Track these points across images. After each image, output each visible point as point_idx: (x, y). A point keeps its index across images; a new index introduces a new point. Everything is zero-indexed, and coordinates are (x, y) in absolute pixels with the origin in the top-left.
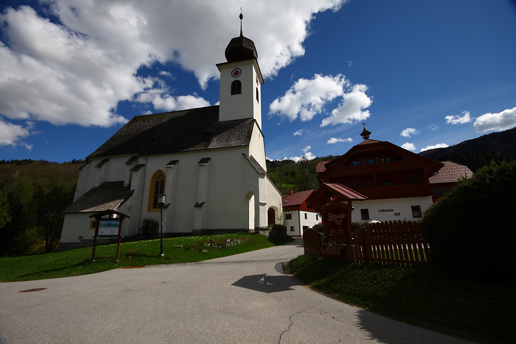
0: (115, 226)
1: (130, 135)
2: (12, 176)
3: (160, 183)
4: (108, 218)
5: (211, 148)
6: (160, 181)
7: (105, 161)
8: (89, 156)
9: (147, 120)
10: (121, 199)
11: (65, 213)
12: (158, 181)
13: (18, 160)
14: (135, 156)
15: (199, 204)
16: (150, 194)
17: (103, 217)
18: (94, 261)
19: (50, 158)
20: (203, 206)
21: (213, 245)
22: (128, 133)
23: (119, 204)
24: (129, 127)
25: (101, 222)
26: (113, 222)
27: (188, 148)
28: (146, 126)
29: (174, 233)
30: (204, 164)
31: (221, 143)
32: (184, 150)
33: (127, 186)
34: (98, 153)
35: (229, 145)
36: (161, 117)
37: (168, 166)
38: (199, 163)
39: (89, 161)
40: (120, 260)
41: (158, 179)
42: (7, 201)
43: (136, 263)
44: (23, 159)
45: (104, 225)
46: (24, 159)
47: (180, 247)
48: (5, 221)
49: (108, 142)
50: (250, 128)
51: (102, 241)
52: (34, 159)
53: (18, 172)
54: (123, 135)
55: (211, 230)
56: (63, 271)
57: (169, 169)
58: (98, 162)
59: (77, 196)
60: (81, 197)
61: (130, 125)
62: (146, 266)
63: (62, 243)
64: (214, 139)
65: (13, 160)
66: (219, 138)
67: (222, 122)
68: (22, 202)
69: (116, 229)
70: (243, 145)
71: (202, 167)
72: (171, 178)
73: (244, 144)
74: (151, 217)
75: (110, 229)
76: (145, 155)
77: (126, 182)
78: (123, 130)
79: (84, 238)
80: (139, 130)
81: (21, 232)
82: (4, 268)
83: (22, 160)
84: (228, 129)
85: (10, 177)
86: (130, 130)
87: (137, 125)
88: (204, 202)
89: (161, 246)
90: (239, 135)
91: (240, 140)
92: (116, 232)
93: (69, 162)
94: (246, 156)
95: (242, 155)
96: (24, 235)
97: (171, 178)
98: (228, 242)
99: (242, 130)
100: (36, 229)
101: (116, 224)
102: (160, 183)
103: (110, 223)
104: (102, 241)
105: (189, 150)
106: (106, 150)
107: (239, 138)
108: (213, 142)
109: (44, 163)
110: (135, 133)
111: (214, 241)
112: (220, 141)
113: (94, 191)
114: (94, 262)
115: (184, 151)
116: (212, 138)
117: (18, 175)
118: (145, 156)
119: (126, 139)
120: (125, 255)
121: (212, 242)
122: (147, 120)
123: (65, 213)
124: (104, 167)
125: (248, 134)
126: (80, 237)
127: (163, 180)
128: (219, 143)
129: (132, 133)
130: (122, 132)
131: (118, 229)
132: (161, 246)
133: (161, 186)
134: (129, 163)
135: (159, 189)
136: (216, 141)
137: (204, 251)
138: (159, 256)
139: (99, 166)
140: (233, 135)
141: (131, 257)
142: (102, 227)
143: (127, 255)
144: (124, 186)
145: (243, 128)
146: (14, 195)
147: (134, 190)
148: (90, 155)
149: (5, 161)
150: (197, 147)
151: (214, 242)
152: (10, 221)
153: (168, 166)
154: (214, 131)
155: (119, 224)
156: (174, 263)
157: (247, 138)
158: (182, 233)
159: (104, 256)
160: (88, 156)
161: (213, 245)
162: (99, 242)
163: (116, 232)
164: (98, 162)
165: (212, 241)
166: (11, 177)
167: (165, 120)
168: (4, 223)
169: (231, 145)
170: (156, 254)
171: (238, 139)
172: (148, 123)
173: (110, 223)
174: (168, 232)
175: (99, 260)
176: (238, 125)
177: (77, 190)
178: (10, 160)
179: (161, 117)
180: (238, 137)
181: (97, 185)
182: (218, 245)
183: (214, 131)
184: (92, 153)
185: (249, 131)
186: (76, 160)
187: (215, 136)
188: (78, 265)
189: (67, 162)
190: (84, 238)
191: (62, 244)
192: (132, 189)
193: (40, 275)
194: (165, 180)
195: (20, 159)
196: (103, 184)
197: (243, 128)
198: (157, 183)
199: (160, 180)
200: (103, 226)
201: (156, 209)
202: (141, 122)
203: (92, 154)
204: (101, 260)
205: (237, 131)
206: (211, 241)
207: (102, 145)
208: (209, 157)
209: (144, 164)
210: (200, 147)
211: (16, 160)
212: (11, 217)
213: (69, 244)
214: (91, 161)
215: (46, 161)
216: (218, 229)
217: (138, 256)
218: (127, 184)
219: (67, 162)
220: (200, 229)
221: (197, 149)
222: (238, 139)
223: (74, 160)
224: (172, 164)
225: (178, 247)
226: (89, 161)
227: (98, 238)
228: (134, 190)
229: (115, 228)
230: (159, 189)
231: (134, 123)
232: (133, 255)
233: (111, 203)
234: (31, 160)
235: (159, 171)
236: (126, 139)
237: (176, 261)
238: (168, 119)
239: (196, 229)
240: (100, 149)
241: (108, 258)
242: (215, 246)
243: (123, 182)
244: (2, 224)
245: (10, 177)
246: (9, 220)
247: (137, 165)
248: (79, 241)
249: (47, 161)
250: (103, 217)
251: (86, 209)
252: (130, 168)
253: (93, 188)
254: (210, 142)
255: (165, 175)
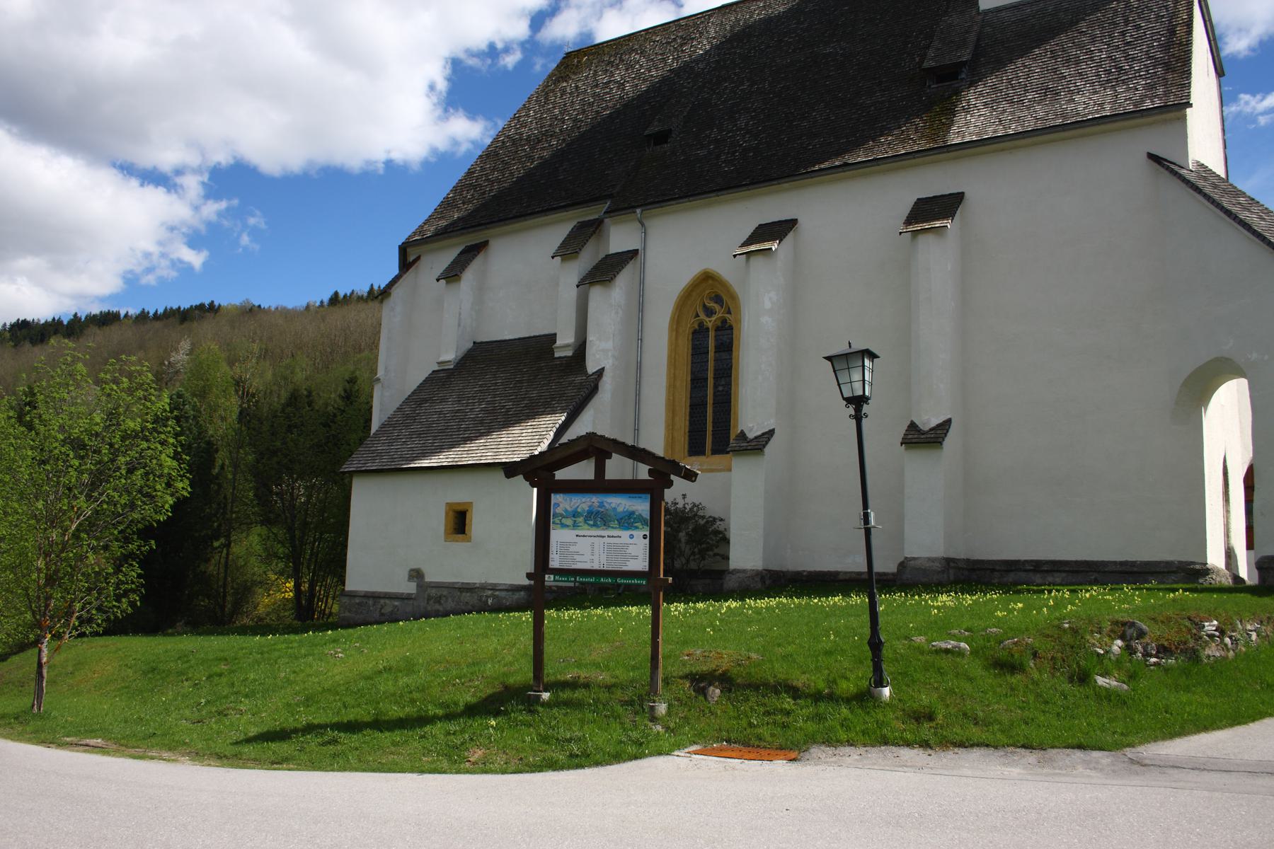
0: (627, 521)
1: (557, 130)
2: (172, 359)
3: (712, 334)
4: (593, 478)
5: (967, 139)
6: (710, 325)
7: (472, 252)
8: (410, 237)
9: (621, 60)
10: (553, 412)
11: (352, 474)
12: (701, 324)
13: (182, 309)
14: (592, 218)
15: (926, 428)
16: (672, 387)
17: (561, 475)
18: (546, 696)
19: (267, 300)
20: (948, 442)
21: (1140, 648)
22: (550, 125)
23: (552, 434)
24: (547, 99)
25: (556, 498)
26: (619, 503)
27: (839, 153)
28: (621, 86)
29: (799, 573)
30: (938, 224)
31: (1012, 113)
32: (822, 166)
33: (569, 353)
34: (443, 223)
35: (1064, 116)
36: (681, 37)
37: (753, 248)
38: (909, 221)
39: (411, 259)
40: (670, 706)
41: (702, 316)
42: (171, 412)
43: (751, 725)
44: (194, 304)
45: (575, 514)
46: (198, 304)
47: (958, 653)
48: (172, 495)
49: (474, 172)
50: (1173, 15)
51: (497, 593)
52: (224, 303)
53: (185, 345)
54: (529, 136)
55: (989, 562)
56: (419, 731)
57: (757, 262)
58: (444, 258)
59: (383, 405)
60: (399, 409)
61: (553, 91)
62: (816, 751)
63: (351, 591)
64: (971, 97)
65: (168, 307)
66: (995, 89)
67: (998, 10)
68: (211, 432)
69: (632, 537)
70: (1148, 104)
71: (926, 241)
72: (768, 305)
73: (1158, 103)
74: (684, 496)
75: (607, 540)
76: (638, 206)
77: (566, 338)
78: (528, 116)
79: (427, 579)
80: (590, 105)
81: (216, 544)
82: (186, 683)
83: (191, 306)
84: (1040, 41)
85: (166, 363)
86: (557, 111)
87: (580, 84)
88: (949, 422)
89: (875, 645)
90: (1114, 60)
91: (1124, 82)
92: (635, 558)
93: (322, 302)
94: (1176, 168)
95: (1151, 162)
96: (228, 554)
97: (768, 305)
98: (1211, 636)
99: (1123, 34)
100: (259, 535)
101: (633, 513)
102: (712, 334)
103: (601, 505)
104: (497, 593)
105: (846, 165)
106: (470, 207)
107: (1115, 77)
108: (966, 111)
109: (251, 311)
110: (575, 120)
111: (1144, 627)
112: (1004, 105)
113: (440, 380)
114: (547, 705)
115: (821, 170)
116: (957, 92)
117: (187, 355)
118: (638, 211)
119: (543, 149)
120: (686, 677)
121: (1130, 631)
122: (621, 60)
123: (352, 474)
124: (469, 276)
125: (1166, 47)
126: (412, 570)
127: (724, 321)
128: (1004, 111)
129: (563, 121)
130: (522, 127)
131: (647, 541)
132: (875, 645)
133: (718, 349)
134: (568, 250)
135: (711, 365)
136: (986, 104)
137: (1101, 681)
138: (865, 698)
139: (452, 275)
140: (1077, 63)
141: (718, 691)
142: (564, 526)
143: (700, 681)
144: (557, 355)
145: (1127, 22)
146: (187, 406)
147: (600, 373)
148: (415, 234)
149: (148, 313)
150: (887, 146)
151: (1141, 634)
152: (186, 494)
153: (753, 248)
154: (966, 55)
155: (647, 515)
156: (972, 746)
157: (1168, 67)
158: (837, 573)
159: (583, 674)
160: (407, 236)
161: (1140, 648)
162: (487, 597)
163: (635, 558)
164: (444, 258)
165: (1133, 624)
166: (169, 363)
167: (702, 47)
168: (171, 501)
169: (1078, 114)
170: (847, 687)
171: (1108, 81)
172: (627, 70)
173: (601, 505)
174: (771, 568)
175: (565, 695)
176: (1098, 10)
177: (378, 380)
178: (161, 311)
179: (681, 37)
180: (1108, 72)
181: (450, 355)
182: (1163, 651)
183: (966, 55)
184: (421, 227)
185: (1172, 32)
186: (341, 295)
187: (973, 84)
188: (472, 711)
189: (316, 302)
190: (427, 579)
191: (352, 595)
192: (591, 368)
193: (329, 743)
194: (739, 321)
195: (185, 305)
196: (470, 351)
197: (1127, 22)
198: (699, 333)
199: (710, 322)
200: (569, 522)
201: (702, 458)
202: (596, 72)
203: (421, 230)
204: (578, 694)
205: (1093, 41)
206: (1124, 624)
207: (455, 190)
208: (960, 191)
209: (633, 254)
210: (903, 141)
211: (177, 307)
212: (188, 478)
213: (375, 596)
214: (418, 258)
215: (257, 304)
216: (1026, 561)
217: (755, 687)
218: (567, 346)
219: (316, 302)
220: (934, 555)
221: (890, 154)
222: (1108, 81)
223: (336, 294)
224: (772, 238)
225: (947, 651)
226: (411, 259)
227: (549, 578)
228: (603, 369)
229: (627, 533)
230: (711, 365)
231: (566, 78)
232: (725, 680)
233: (516, 430)
234: (216, 304)
235: (707, 278)
236: (543, 149)
237: (975, 732)
238: (714, 38)
239: (914, 559)
240: (447, 204)
241: (609, 688)
242: (1147, 654)
243: (552, 338)
244: (163, 507)
245: (166, 363)
246: (183, 487)
247: (602, 256)
248: (410, 588)
249: (259, 306)
250: (561, 475)
251: (424, 455)
252: (572, 272)
253: (436, 368)
254: (954, 113)
255: (734, 297)
